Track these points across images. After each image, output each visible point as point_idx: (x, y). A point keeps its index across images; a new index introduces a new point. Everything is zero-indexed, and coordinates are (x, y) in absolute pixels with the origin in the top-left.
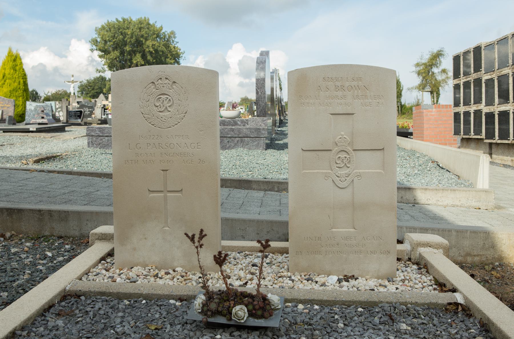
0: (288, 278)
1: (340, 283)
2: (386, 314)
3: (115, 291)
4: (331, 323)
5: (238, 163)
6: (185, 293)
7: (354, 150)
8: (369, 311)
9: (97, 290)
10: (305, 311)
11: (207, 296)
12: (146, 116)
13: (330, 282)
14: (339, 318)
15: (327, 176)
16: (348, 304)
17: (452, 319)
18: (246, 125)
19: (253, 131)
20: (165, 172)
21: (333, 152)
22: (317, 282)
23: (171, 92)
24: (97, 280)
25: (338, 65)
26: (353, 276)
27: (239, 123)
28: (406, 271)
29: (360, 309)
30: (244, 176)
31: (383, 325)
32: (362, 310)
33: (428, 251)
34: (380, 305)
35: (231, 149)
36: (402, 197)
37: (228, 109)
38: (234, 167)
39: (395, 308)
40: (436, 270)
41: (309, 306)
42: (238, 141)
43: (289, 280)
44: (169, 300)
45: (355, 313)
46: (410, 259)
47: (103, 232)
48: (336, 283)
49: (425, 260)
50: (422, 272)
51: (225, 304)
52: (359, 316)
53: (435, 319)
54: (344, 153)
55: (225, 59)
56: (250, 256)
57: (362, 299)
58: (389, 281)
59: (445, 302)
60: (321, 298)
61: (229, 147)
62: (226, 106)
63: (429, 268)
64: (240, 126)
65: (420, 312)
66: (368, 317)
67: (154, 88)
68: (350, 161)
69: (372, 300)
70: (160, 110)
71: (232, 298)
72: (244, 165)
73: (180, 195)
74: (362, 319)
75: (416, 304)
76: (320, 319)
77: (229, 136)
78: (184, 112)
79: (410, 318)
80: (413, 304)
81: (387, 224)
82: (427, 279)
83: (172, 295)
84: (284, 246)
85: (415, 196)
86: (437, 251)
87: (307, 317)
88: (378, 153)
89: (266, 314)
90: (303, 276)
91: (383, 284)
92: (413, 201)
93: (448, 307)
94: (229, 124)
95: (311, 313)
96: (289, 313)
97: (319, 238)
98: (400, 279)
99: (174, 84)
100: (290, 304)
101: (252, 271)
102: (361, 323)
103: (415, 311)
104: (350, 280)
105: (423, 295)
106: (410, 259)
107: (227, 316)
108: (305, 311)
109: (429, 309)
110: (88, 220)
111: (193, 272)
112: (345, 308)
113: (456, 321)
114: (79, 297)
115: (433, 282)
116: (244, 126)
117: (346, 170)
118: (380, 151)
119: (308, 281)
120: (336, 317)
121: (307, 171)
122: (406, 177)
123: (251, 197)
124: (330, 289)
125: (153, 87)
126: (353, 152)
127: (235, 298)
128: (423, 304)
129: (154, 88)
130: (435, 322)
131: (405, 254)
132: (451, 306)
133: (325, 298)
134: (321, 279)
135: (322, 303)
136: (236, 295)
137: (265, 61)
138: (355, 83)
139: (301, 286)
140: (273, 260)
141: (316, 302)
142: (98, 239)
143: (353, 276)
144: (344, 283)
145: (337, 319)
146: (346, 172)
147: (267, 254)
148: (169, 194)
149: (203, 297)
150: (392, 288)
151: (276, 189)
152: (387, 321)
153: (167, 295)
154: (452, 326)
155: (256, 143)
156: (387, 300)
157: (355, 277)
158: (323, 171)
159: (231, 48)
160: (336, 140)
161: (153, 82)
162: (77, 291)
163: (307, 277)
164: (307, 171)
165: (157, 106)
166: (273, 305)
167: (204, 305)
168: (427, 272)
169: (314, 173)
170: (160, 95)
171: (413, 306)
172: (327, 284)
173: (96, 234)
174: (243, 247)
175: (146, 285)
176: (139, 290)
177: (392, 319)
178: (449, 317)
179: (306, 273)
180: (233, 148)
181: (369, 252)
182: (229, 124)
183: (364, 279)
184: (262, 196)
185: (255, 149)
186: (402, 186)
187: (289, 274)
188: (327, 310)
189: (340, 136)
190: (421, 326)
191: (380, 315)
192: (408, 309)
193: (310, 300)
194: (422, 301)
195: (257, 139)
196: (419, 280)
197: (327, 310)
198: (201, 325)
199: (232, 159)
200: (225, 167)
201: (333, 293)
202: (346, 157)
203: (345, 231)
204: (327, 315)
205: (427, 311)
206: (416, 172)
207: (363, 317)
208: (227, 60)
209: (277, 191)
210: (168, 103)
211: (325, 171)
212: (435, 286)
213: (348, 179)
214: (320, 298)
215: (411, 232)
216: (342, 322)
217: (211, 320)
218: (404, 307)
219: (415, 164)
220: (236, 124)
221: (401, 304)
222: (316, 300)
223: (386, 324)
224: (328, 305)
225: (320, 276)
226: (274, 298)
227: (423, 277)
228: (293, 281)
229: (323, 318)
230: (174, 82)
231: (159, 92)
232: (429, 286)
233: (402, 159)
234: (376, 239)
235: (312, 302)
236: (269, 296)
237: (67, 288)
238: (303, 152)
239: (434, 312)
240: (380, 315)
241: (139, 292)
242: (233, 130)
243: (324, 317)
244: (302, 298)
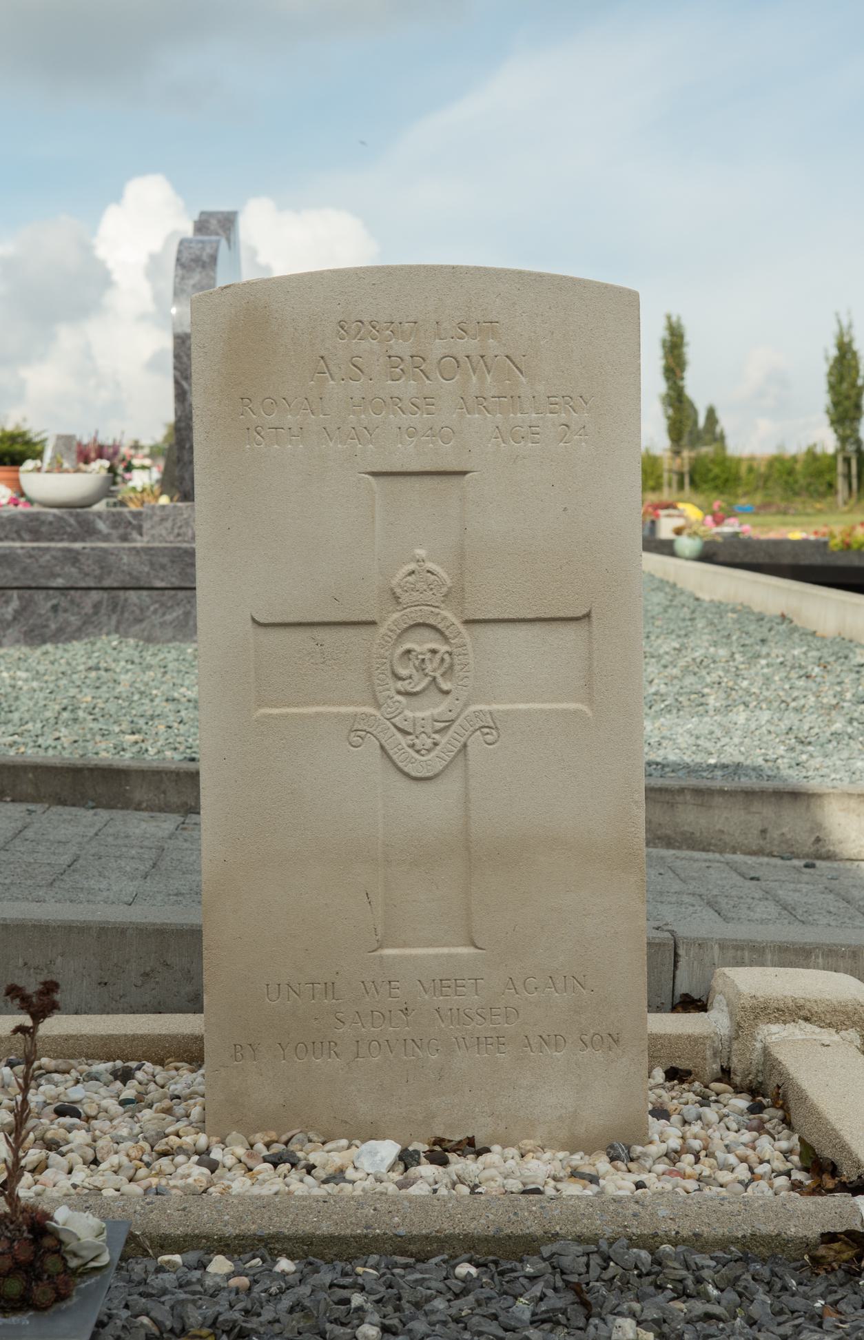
0: (196, 1158)
1: (406, 1169)
2: (567, 1283)
4: (328, 1326)
5: (87, 698)
7: (468, 622)
8: (502, 1273)
10: (234, 1282)
13: (366, 1165)
14: (369, 1306)
15: (356, 730)
16: (418, 1249)
17: (831, 1298)
18: (135, 535)
19: (165, 560)
21: (383, 630)
22: (310, 1169)
25: (402, 268)
26: (471, 1142)
27: (102, 526)
28: (699, 1118)
29: (464, 1269)
30: (104, 753)
31: (547, 1326)
32: (474, 1271)
33: (799, 1035)
34: (546, 1251)
35: (68, 640)
36: (764, 831)
37: (57, 468)
38: (65, 715)
39: (607, 1259)
40: (813, 1111)
41: (257, 1261)
42: (97, 606)
43: (199, 1163)
45: (441, 1286)
46: (725, 1074)
48: (391, 1169)
49: (781, 1074)
50: (762, 1122)
52: (457, 1296)
53: (761, 1296)
54: (427, 633)
55: (87, 249)
56: (56, 1076)
57: (476, 1227)
58: (612, 1159)
59: (814, 1231)
60: (308, 1229)
61: (60, 630)
62: (48, 455)
63: (792, 1104)
64: (106, 538)
65: (706, 1273)
66: (489, 1299)
68: (451, 667)
69: (517, 1230)
72: (111, 707)
74: (464, 1306)
75: (697, 1242)
76: (291, 1310)
77: (60, 582)
79: (660, 1298)
80: (684, 1241)
81: (612, 920)
82: (773, 1149)
85: (818, 826)
86: (836, 1038)
87: (239, 1306)
88: (569, 631)
89: (41, 1292)
90: (260, 1146)
91: (587, 1170)
92: (809, 848)
93: (822, 1251)
94: (57, 530)
95: (257, 1288)
96: (164, 1292)
97: (330, 988)
98: (663, 1148)
100: (177, 1258)
101: (49, 1135)
102: (457, 1321)
103: (687, 1268)
104: (452, 1157)
105: (727, 1207)
106: (725, 1074)
108: (234, 1282)
109: (745, 1259)
112: (406, 1267)
113: (842, 1306)
115: (795, 1158)
116: (124, 538)
117: (436, 705)
118: (573, 625)
119: (275, 1165)
120: (357, 1299)
121: (275, 711)
122: (792, 749)
123: (116, 836)
124: (358, 1192)
126: (462, 628)
128: (724, 1243)
130: (755, 1310)
131: (709, 1053)
132: (836, 1246)
133: (326, 1228)
134: (325, 1157)
135: (311, 1249)
137: (214, 259)
138: (469, 345)
139: (239, 1184)
140: (152, 1086)
141: (288, 1246)
143: (471, 1142)
144: (427, 1170)
145: (359, 1309)
146: (436, 711)
147: (134, 1064)
150: (618, 1182)
152: (564, 1312)
154: (820, 1325)
155: (178, 612)
156: (578, 1229)
157: (478, 1146)
158: (343, 709)
159: (117, 196)
160: (394, 582)
163: (277, 1148)
164: (275, 711)
166: (75, 1255)
168: (787, 1122)
169: (302, 716)
171: (681, 1248)
172: (350, 1173)
177: (585, 1304)
178: (820, 1289)
179: (273, 1135)
180: (77, 635)
181: (534, 1041)
182: (57, 530)
183: (512, 1151)
184: (166, 834)
185: (174, 638)
186: (766, 784)
187: (202, 1140)
188: (326, 1276)
189: (412, 566)
190: (699, 1326)
191: (537, 1290)
192: (657, 1262)
193: (261, 1239)
194: (721, 1231)
195: (181, 594)
196: (741, 1151)
197: (326, 1276)
199: (63, 682)
200: (27, 716)
201: (360, 1206)
202: (434, 652)
203: (436, 956)
204: (322, 1295)
205: (737, 1269)
206: (837, 726)
207: (471, 1298)
208: (101, 252)
211: (351, 709)
212: (798, 1176)
213: (443, 740)
214: (305, 1228)
215: (740, 963)
216: (376, 1318)
218: (644, 1254)
219: (839, 695)
220: (87, 530)
221: (635, 1242)
222: (289, 1238)
223: (558, 1323)
224: (338, 1256)
225: (329, 1146)
226: (79, 1226)
227: (765, 1140)
228: (213, 1166)
229: (304, 1309)
232: (780, 1174)
233: (793, 675)
234: (560, 985)
235: (270, 1245)
236: (62, 1216)
238: (261, 631)
239: (765, 1272)
240: (537, 1290)
242: (73, 557)
243: (307, 1303)
244: (230, 1231)
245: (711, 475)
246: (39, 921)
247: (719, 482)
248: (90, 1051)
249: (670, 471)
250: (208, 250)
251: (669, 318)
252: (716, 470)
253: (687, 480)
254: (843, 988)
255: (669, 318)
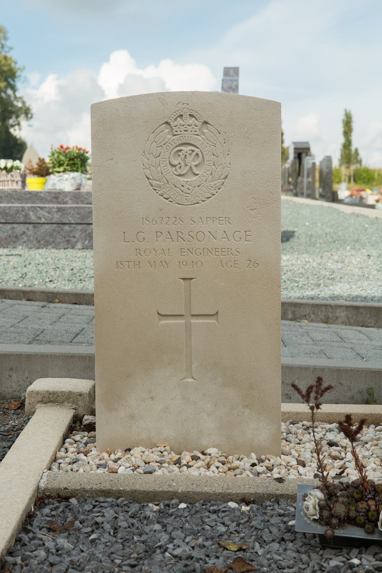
3: (128, 489)
6: (252, 491)
9: (95, 487)
11: (326, 491)
12: (154, 182)
20: (188, 282)
23: (199, 140)
24: (81, 471)
44: (228, 501)
47: (51, 390)
51: (361, 506)
67: (169, 133)
70: (180, 172)
71: (370, 496)
73: (215, 321)
78: (223, 176)
83: (229, 494)
84: (369, 412)
99: (205, 126)
107: (367, 526)
110: (11, 369)
111: (237, 456)
114: (67, 499)
125: (167, 131)
127: (374, 496)
129: (169, 133)
136: (375, 490)
142: (41, 402)
148: (194, 321)
149: (319, 494)
151: (290, 316)
153: (220, 494)
161: (167, 123)
162: (60, 489)
165: (174, 166)
167: (322, 508)
170: (180, 145)
173: (38, 393)
174: (298, 414)
175: (168, 477)
176: (170, 486)
198: (313, 542)
209: (291, 320)
210: (193, 160)
217: (340, 533)
230: (206, 123)
231: (177, 140)
237: (42, 485)
241: (171, 489)
245: (362, 177)
246: (289, 365)
247: (366, 180)
248: (321, 419)
249: (345, 175)
250: (235, 83)
251: (346, 110)
252: (364, 175)
253: (352, 179)
254: (377, 409)
255: (346, 110)
